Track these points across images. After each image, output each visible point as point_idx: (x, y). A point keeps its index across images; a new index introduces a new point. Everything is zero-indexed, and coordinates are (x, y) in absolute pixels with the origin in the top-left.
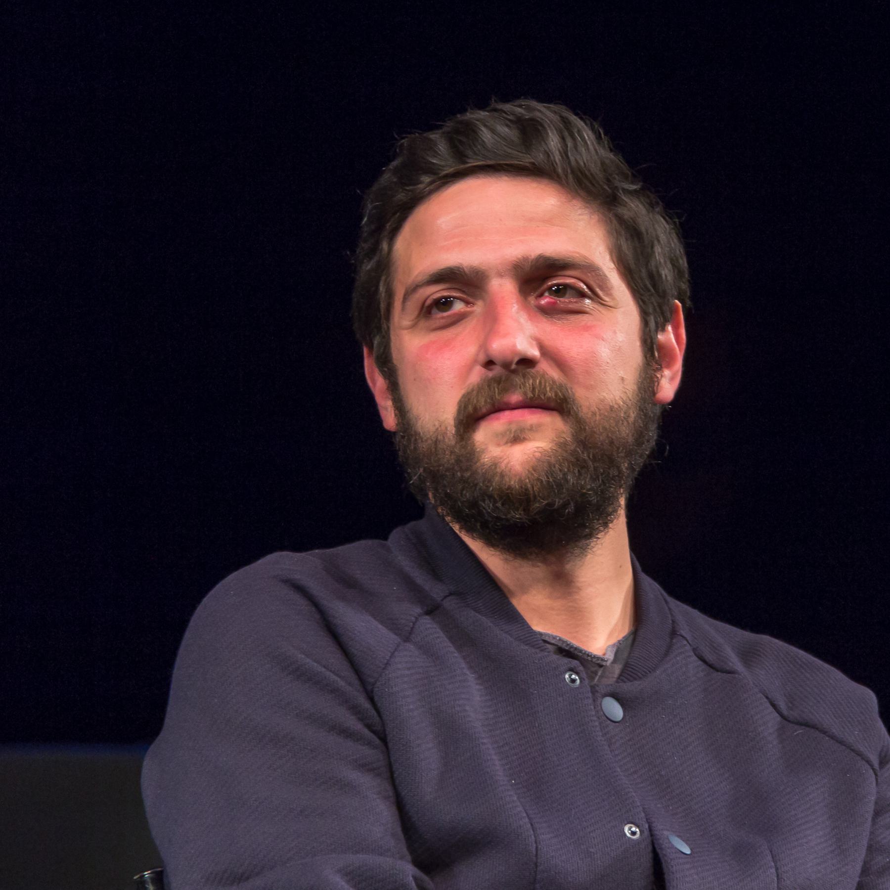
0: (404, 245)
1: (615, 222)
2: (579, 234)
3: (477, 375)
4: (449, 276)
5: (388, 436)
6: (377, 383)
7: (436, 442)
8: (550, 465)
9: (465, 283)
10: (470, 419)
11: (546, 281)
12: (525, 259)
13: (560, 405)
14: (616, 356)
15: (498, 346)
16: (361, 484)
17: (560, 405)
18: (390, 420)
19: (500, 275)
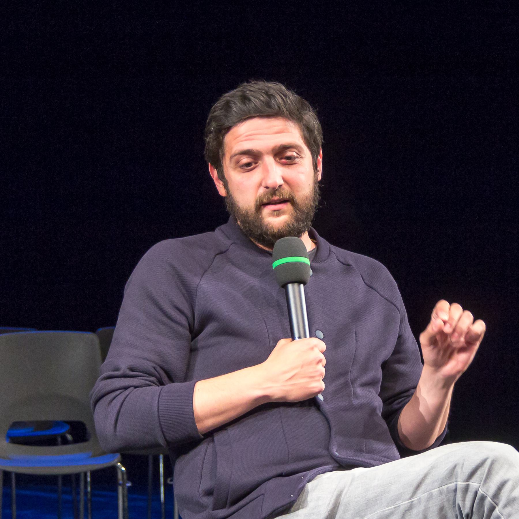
0: (228, 138)
1: (305, 130)
2: (291, 134)
3: (262, 190)
4: (247, 153)
5: (222, 199)
6: (214, 174)
7: (247, 212)
8: (288, 224)
9: (254, 157)
10: (261, 205)
11: (283, 154)
12: (276, 146)
13: (291, 200)
14: (305, 175)
15: (270, 182)
16: (211, 211)
17: (291, 200)
18: (222, 192)
19: (268, 153)
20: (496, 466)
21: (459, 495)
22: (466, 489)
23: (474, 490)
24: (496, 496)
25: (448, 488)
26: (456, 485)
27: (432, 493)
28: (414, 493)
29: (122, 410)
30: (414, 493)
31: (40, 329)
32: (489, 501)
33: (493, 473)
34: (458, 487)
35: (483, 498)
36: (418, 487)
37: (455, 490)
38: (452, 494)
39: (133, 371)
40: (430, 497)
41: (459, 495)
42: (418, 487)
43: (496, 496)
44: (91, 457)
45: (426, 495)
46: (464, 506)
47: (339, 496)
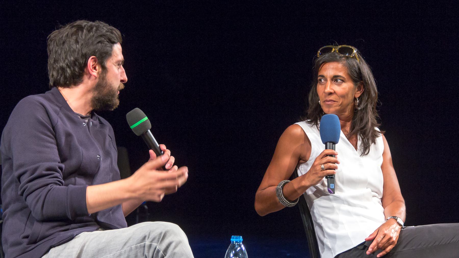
20: (168, 235)
21: (146, 249)
22: (150, 246)
23: (155, 247)
24: (166, 251)
25: (140, 245)
26: (145, 244)
27: (131, 248)
28: (123, 247)
29: (48, 196)
30: (123, 247)
31: (6, 123)
32: (161, 252)
33: (166, 238)
34: (146, 245)
35: (158, 251)
36: (125, 244)
37: (144, 246)
38: (143, 249)
39: (367, 105)
40: (131, 250)
41: (146, 249)
42: (125, 244)
43: (166, 251)
44: (129, 239)
45: (129, 248)
46: (148, 256)
47: (83, 247)
